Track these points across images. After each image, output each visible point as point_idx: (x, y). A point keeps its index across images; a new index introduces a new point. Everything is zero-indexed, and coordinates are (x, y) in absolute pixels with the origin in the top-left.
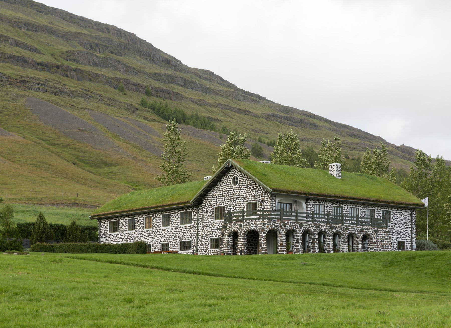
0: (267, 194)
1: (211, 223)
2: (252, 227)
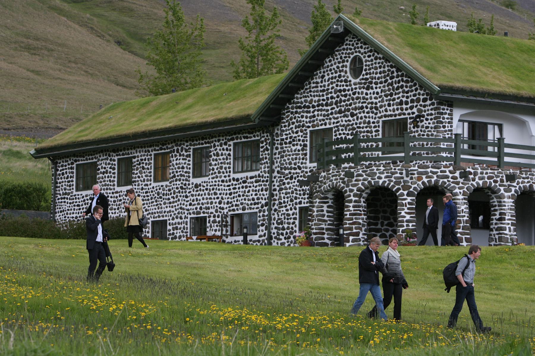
0: (431, 100)
1: (300, 168)
2: (380, 178)
